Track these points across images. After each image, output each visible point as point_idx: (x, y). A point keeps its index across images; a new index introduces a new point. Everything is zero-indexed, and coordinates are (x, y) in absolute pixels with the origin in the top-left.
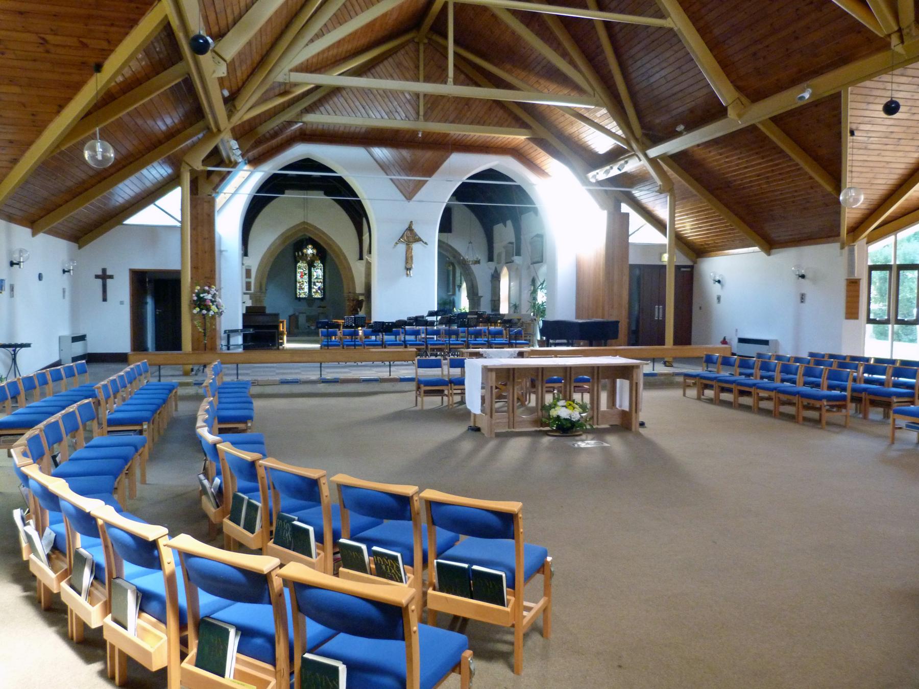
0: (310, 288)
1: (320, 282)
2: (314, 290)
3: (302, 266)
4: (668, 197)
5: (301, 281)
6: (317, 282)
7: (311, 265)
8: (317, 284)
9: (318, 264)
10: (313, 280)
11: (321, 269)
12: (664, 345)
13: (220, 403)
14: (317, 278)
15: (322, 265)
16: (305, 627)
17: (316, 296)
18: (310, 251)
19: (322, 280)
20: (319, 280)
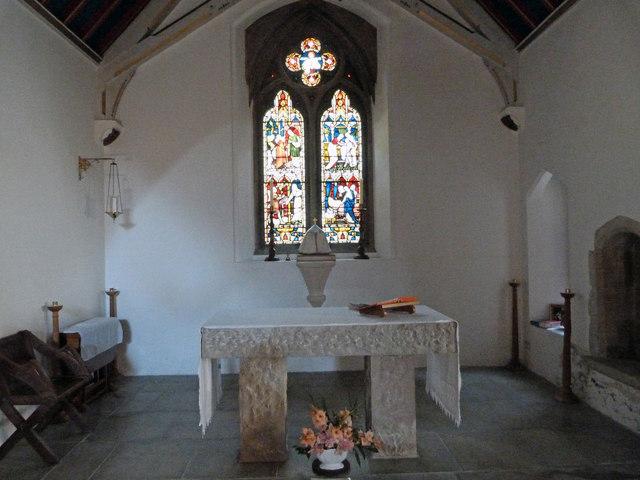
0: (314, 207)
1: (353, 181)
2: (327, 216)
3: (283, 113)
4: (415, 424)
5: (278, 177)
6: (342, 182)
7: (312, 104)
8: (341, 189)
9: (341, 111)
10: (325, 176)
11: (354, 131)
12: (197, 376)
13: (281, 122)
14: (336, 167)
15: (356, 115)
16: (128, 25)
17: (337, 239)
18: (310, 62)
19: (358, 175)
20: (348, 175)
